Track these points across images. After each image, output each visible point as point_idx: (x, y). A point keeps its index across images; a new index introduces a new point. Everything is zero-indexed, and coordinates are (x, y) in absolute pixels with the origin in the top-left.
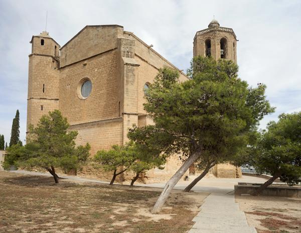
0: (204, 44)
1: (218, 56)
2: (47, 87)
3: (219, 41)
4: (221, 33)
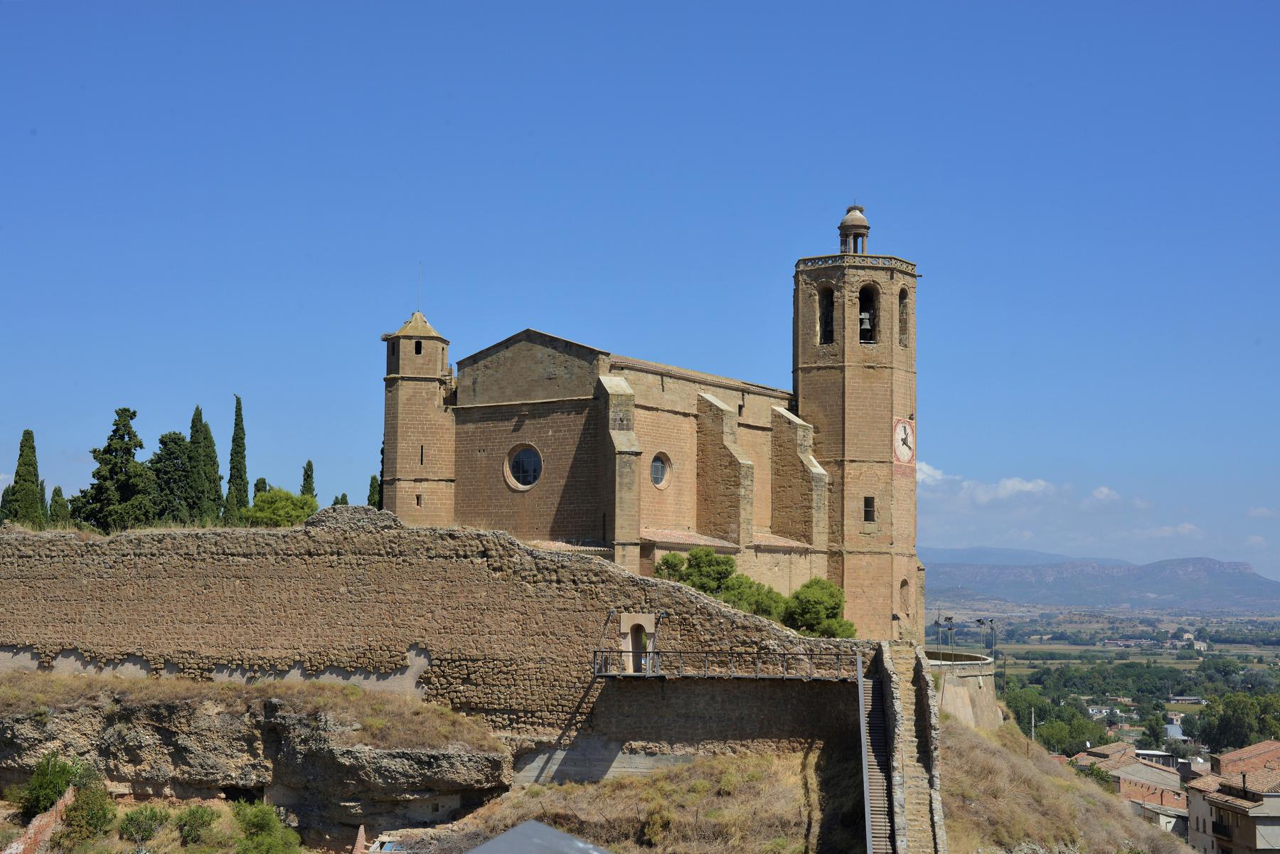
4: (861, 272)
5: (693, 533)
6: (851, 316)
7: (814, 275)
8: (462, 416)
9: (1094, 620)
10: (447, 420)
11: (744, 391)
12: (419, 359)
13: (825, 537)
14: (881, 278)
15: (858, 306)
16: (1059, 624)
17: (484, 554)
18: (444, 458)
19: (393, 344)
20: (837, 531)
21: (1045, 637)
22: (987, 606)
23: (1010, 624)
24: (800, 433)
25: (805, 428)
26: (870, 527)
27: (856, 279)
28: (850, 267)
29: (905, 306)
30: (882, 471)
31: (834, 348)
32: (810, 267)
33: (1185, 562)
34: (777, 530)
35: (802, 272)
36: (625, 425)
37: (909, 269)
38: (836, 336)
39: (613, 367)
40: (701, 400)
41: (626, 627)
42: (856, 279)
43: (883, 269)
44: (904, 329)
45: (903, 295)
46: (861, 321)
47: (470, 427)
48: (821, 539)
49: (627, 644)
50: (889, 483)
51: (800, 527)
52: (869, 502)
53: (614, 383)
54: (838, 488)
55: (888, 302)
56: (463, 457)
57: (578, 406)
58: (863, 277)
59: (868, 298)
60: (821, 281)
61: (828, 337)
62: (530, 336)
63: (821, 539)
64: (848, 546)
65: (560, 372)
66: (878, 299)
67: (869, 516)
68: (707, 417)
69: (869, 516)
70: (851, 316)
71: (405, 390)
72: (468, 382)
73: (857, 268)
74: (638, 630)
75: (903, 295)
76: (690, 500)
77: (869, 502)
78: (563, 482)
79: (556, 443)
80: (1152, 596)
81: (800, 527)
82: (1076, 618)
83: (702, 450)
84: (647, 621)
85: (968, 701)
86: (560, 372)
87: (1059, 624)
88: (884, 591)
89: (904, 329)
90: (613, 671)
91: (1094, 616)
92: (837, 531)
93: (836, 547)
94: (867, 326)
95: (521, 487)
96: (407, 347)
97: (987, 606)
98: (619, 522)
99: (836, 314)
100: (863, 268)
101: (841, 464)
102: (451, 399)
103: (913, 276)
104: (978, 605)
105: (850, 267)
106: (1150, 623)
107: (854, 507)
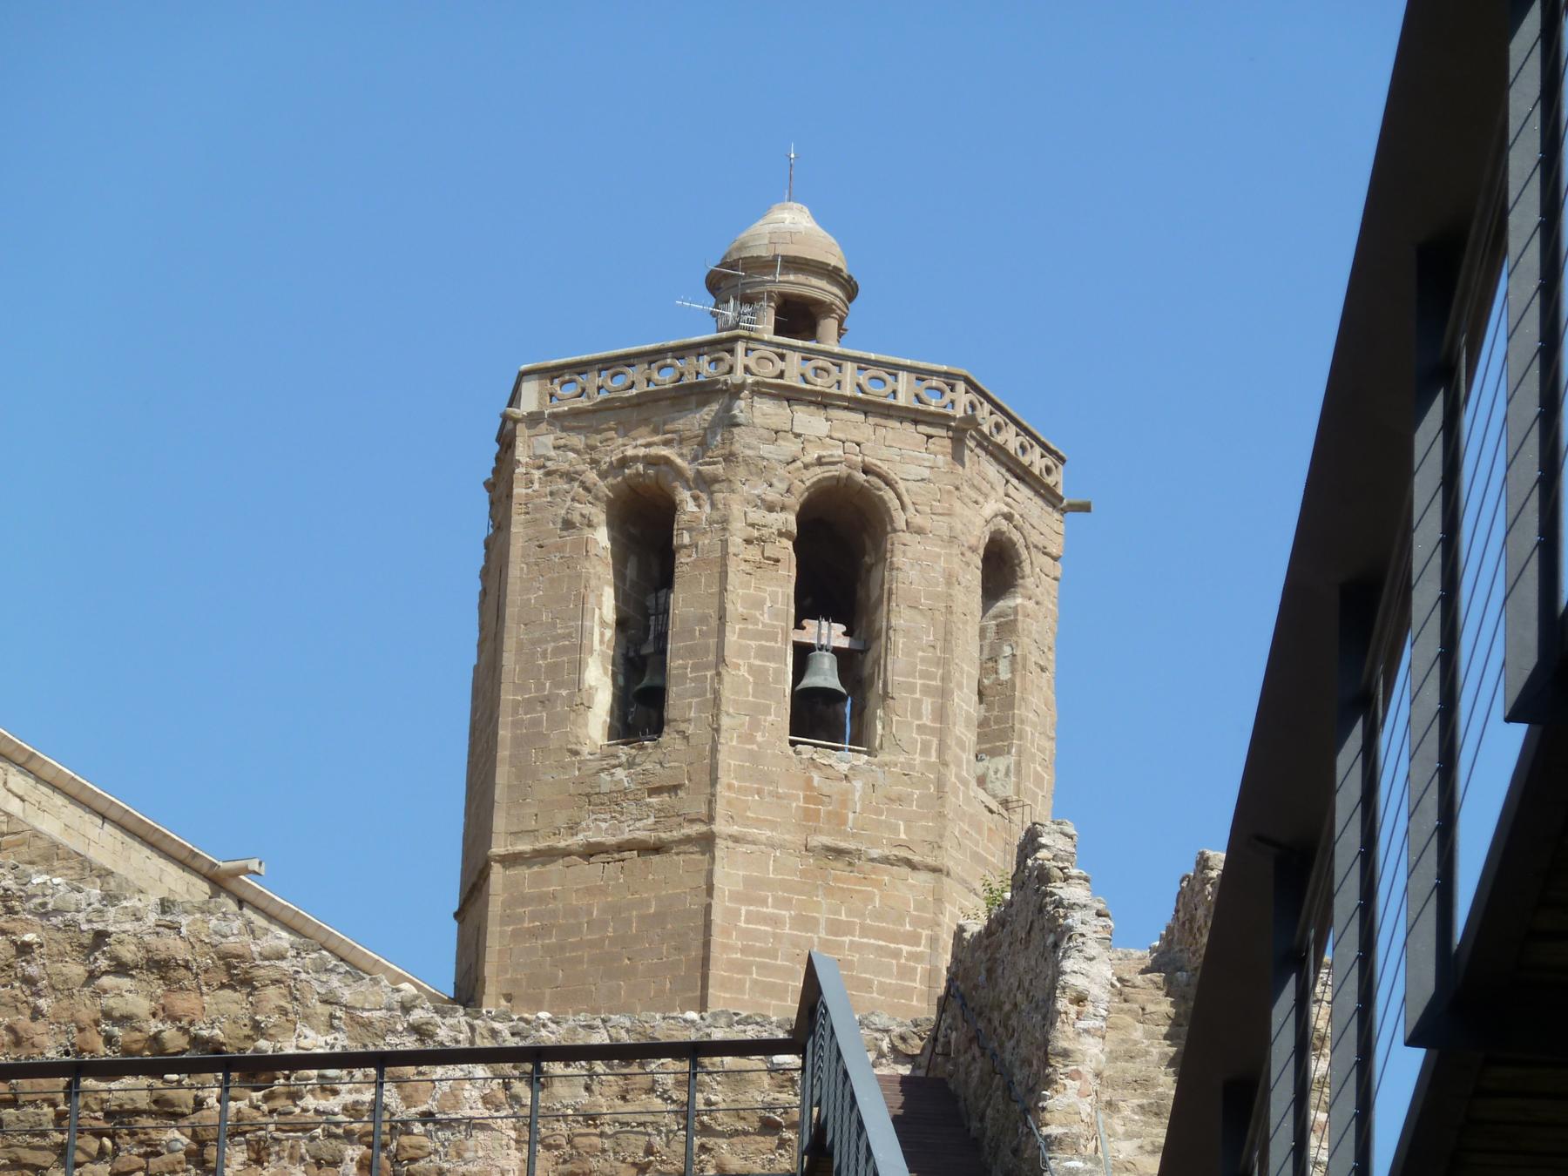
0: (602, 537)
1: (756, 712)
3: (790, 521)
4: (810, 421)
6: (747, 612)
14: (906, 462)
15: (788, 572)
27: (786, 450)
28: (760, 390)
29: (1007, 628)
31: (666, 755)
32: (568, 397)
35: (575, 619)
37: (1035, 460)
38: (680, 701)
43: (916, 417)
46: (803, 654)
55: (926, 573)
58: (821, 443)
59: (838, 551)
61: (642, 709)
66: (881, 555)
70: (747, 612)
73: (791, 396)
85: (843, 845)
94: (825, 675)
99: (684, 603)
100: (823, 402)
103: (1050, 496)
105: (760, 390)
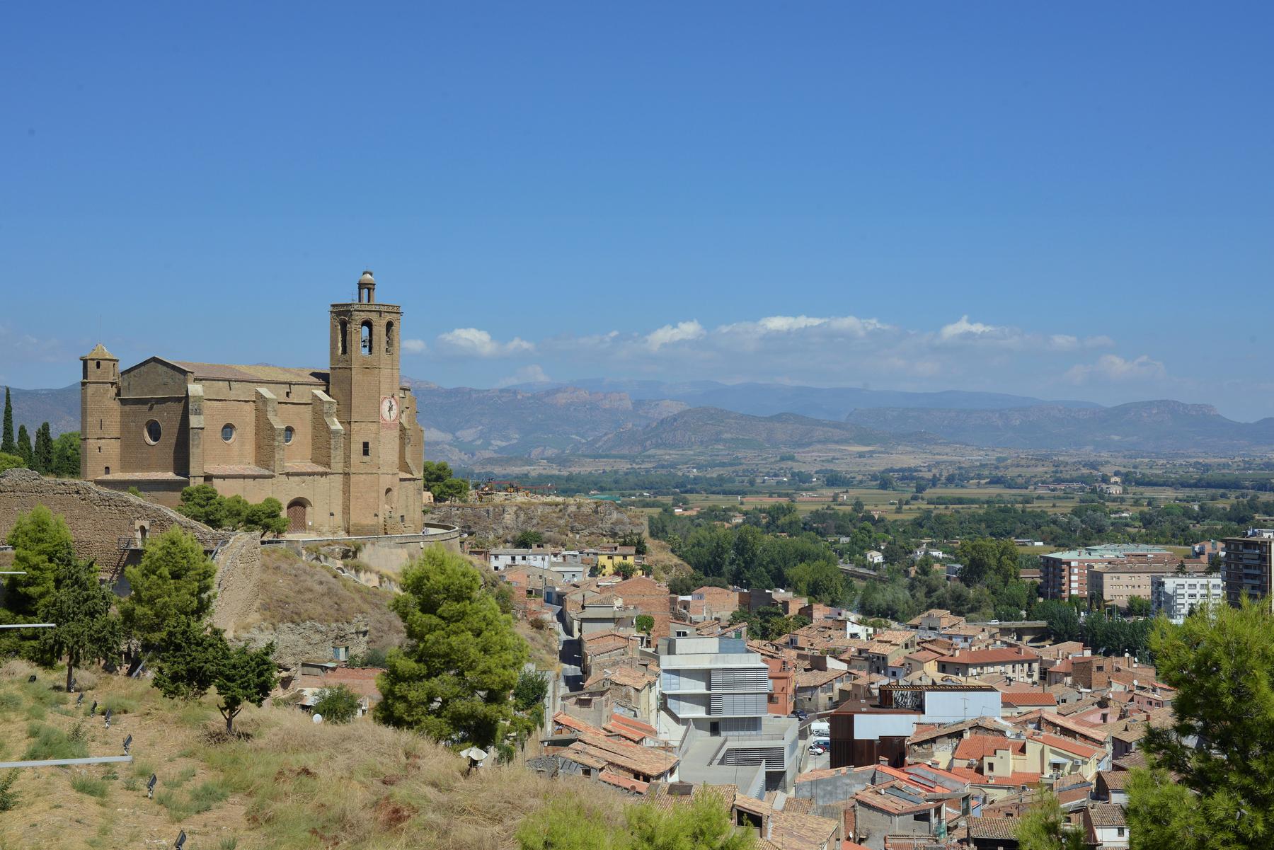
2: (106, 423)
5: (253, 466)
7: (338, 314)
8: (124, 402)
9: (1040, 463)
10: (116, 405)
11: (290, 384)
12: (99, 371)
13: (342, 465)
14: (374, 317)
16: (1006, 468)
17: (78, 492)
18: (114, 427)
19: (85, 362)
20: (347, 460)
21: (983, 482)
22: (948, 450)
23: (960, 468)
24: (327, 406)
25: (330, 403)
26: (366, 458)
27: (359, 317)
30: (373, 427)
33: (1150, 404)
34: (315, 461)
36: (198, 412)
39: (196, 380)
40: (257, 393)
41: (137, 527)
42: (359, 317)
44: (390, 343)
45: (390, 325)
47: (127, 408)
48: (338, 465)
49: (139, 535)
50: (378, 433)
51: (326, 459)
52: (366, 445)
53: (195, 389)
54: (348, 436)
55: (379, 330)
56: (124, 426)
57: (178, 400)
60: (342, 315)
62: (154, 360)
63: (338, 465)
64: (353, 470)
65: (170, 381)
67: (366, 452)
68: (260, 400)
69: (366, 452)
71: (91, 389)
72: (126, 384)
74: (143, 529)
75: (390, 325)
76: (250, 448)
77: (366, 445)
78: (174, 441)
79: (167, 418)
80: (1116, 438)
81: (326, 459)
82: (1023, 462)
83: (257, 420)
84: (146, 524)
86: (170, 381)
87: (1006, 468)
88: (374, 495)
89: (390, 343)
90: (133, 547)
91: (1041, 459)
92: (347, 460)
93: (347, 470)
95: (152, 443)
96: (92, 365)
97: (948, 450)
98: (191, 465)
101: (350, 423)
102: (118, 394)
104: (938, 449)
106: (1093, 466)
107: (357, 448)
